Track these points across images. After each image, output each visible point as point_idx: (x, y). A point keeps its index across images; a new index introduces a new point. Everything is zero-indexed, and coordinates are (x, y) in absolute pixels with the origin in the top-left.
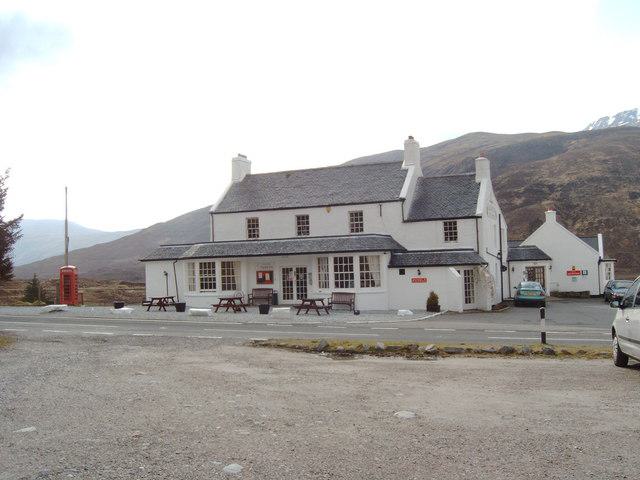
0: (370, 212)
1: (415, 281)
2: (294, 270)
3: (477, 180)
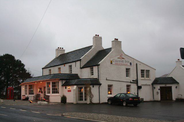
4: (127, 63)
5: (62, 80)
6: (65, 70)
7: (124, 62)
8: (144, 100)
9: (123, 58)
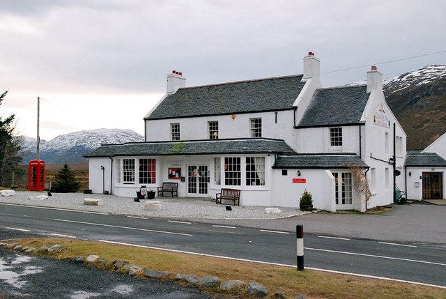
0: (267, 118)
1: (295, 181)
2: (198, 168)
3: (368, 91)
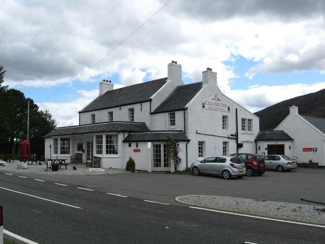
1: (135, 151)
4: (223, 108)
5: (124, 132)
6: (121, 115)
7: (220, 105)
8: (319, 165)
9: (219, 100)
